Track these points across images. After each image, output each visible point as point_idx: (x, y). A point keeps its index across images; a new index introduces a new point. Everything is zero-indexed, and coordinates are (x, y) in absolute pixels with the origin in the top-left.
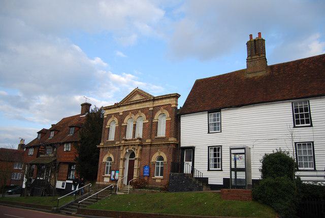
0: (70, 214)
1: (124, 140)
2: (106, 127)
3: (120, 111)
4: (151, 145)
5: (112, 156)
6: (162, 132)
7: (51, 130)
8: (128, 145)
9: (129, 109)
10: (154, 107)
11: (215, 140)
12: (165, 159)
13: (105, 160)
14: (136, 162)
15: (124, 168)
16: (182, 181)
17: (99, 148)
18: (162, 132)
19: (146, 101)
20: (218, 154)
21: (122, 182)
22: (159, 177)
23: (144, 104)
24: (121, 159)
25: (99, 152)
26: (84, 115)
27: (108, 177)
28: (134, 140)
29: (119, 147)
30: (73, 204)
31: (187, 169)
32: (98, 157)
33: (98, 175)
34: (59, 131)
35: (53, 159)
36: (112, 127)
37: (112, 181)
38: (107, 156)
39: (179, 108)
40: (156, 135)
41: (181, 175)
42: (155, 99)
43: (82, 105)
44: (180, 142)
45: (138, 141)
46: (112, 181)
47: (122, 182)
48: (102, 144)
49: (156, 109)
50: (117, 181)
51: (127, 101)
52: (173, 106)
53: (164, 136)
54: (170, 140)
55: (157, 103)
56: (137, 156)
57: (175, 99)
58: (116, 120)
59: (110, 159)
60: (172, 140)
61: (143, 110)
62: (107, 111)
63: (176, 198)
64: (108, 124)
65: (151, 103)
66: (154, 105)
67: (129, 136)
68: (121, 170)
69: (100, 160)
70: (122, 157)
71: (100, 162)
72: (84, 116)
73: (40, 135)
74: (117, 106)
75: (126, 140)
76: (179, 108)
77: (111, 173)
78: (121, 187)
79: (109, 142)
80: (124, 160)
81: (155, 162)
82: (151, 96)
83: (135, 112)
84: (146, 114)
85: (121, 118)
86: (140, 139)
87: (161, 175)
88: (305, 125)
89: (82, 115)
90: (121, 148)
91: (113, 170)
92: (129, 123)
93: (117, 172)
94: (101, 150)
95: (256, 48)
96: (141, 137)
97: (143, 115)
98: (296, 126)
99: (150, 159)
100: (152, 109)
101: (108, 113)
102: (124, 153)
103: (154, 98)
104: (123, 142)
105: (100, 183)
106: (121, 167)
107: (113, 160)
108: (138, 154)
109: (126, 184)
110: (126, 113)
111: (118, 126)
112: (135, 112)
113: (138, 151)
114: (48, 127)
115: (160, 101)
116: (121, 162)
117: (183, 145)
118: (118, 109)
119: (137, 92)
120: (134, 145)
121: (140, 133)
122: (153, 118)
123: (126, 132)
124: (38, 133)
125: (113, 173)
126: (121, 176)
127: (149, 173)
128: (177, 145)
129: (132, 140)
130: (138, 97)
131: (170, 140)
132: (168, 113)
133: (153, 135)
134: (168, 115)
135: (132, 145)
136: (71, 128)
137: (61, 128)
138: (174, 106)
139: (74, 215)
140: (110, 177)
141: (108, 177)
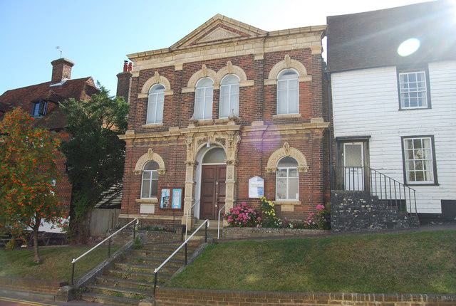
2: (140, 96)
3: (178, 62)
5: (158, 159)
6: (289, 103)
9: (226, 55)
10: (265, 55)
11: (416, 122)
13: (140, 166)
18: (289, 103)
20: (410, 146)
24: (190, 164)
27: (150, 203)
31: (353, 181)
36: (157, 98)
40: (274, 112)
42: (268, 36)
46: (159, 210)
47: (192, 214)
49: (270, 60)
51: (195, 40)
55: (273, 47)
59: (152, 165)
60: (319, 123)
61: (236, 61)
62: (140, 63)
63: (71, 251)
65: (259, 44)
67: (203, 110)
71: (127, 171)
74: (171, 51)
83: (216, 65)
84: (246, 69)
85: (179, 78)
88: (410, 108)
92: (202, 87)
95: (60, 65)
98: (402, 108)
100: (261, 57)
101: (142, 68)
103: (268, 33)
110: (191, 68)
111: (171, 93)
112: (216, 65)
115: (281, 42)
117: (337, 134)
119: (218, 23)
121: (231, 107)
122: (265, 76)
123: (194, 106)
125: (165, 193)
126: (187, 200)
128: (328, 132)
130: (221, 34)
141: (150, 203)
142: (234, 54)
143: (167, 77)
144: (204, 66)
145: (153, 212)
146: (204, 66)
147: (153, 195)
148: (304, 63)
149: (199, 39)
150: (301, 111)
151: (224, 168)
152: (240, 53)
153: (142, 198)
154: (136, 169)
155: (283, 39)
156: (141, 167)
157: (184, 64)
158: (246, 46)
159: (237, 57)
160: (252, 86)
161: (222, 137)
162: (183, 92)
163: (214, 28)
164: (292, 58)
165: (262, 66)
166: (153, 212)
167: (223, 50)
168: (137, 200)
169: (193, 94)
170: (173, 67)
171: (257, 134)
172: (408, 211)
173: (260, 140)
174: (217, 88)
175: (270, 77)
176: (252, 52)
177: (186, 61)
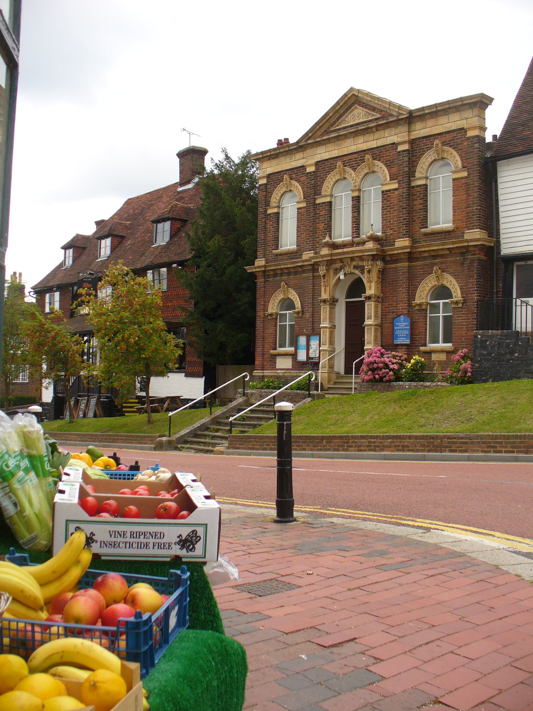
0: (211, 452)
1: (327, 245)
2: (270, 211)
4: (411, 257)
7: (99, 237)
8: (341, 260)
9: (364, 147)
12: (457, 294)
13: (273, 308)
14: (370, 308)
15: (333, 327)
16: (512, 353)
17: (253, 276)
19: (387, 125)
21: (331, 367)
22: (441, 345)
23: (381, 133)
24: (325, 301)
25: (252, 289)
26: (188, 182)
28: (358, 244)
29: (314, 267)
30: (207, 429)
32: (253, 305)
33: (258, 350)
34: (123, 237)
35: (33, 346)
37: (300, 366)
38: (279, 296)
39: (489, 139)
40: (424, 223)
41: (507, 336)
43: (182, 155)
44: (498, 243)
45: (370, 245)
47: (331, 367)
48: (260, 262)
50: (318, 363)
52: (470, 134)
53: (449, 225)
54: (466, 237)
56: (371, 290)
57: (476, 111)
58: (298, 189)
59: (289, 304)
64: (274, 201)
66: (415, 135)
68: (325, 335)
69: (259, 307)
70: (325, 296)
71: (260, 313)
72: (190, 186)
73: (70, 252)
75: (334, 246)
76: (489, 139)
77: (294, 343)
78: (329, 381)
79: (281, 255)
80: (333, 302)
81: (427, 304)
82: (400, 107)
86: (374, 238)
87: (445, 341)
89: (183, 182)
90: (322, 270)
91: (303, 334)
93: (312, 338)
94: (260, 281)
96: (380, 234)
97: (381, 168)
99: (411, 296)
100: (406, 147)
102: (333, 281)
103: (411, 112)
104: (325, 251)
105: (267, 373)
106: (325, 324)
107: (298, 305)
108: (373, 285)
109: (342, 372)
111: (304, 205)
113: (374, 274)
114: (90, 230)
115: (430, 122)
116: (325, 311)
118: (299, 155)
120: (361, 258)
122: (411, 174)
124: (65, 248)
127: (412, 335)
129: (351, 244)
131: (466, 237)
132: (458, 158)
133: (417, 225)
134: (460, 163)
135: (352, 259)
136: (160, 226)
137: (126, 227)
138: (475, 133)
139: (222, 453)
140: (294, 356)
142: (373, 144)
143: (298, 181)
144: (286, 176)
145: (291, 367)
146: (339, 163)
147: (291, 345)
148: (457, 151)
149: (332, 125)
150: (202, 377)
151: (362, 303)
152: (380, 143)
153: (280, 249)
154: (270, 311)
155: (432, 118)
156: (275, 308)
157: (317, 164)
158: (387, 133)
159: (377, 148)
160: (396, 189)
161: (360, 263)
162: (318, 202)
163: (350, 107)
164: (444, 144)
165: (406, 159)
166: (291, 367)
167: (361, 139)
168: (272, 352)
169: (330, 203)
170: (303, 167)
171: (402, 256)
172: (409, 343)
173: (406, 264)
174: (356, 194)
175: (418, 175)
176: (395, 139)
177: (318, 158)
